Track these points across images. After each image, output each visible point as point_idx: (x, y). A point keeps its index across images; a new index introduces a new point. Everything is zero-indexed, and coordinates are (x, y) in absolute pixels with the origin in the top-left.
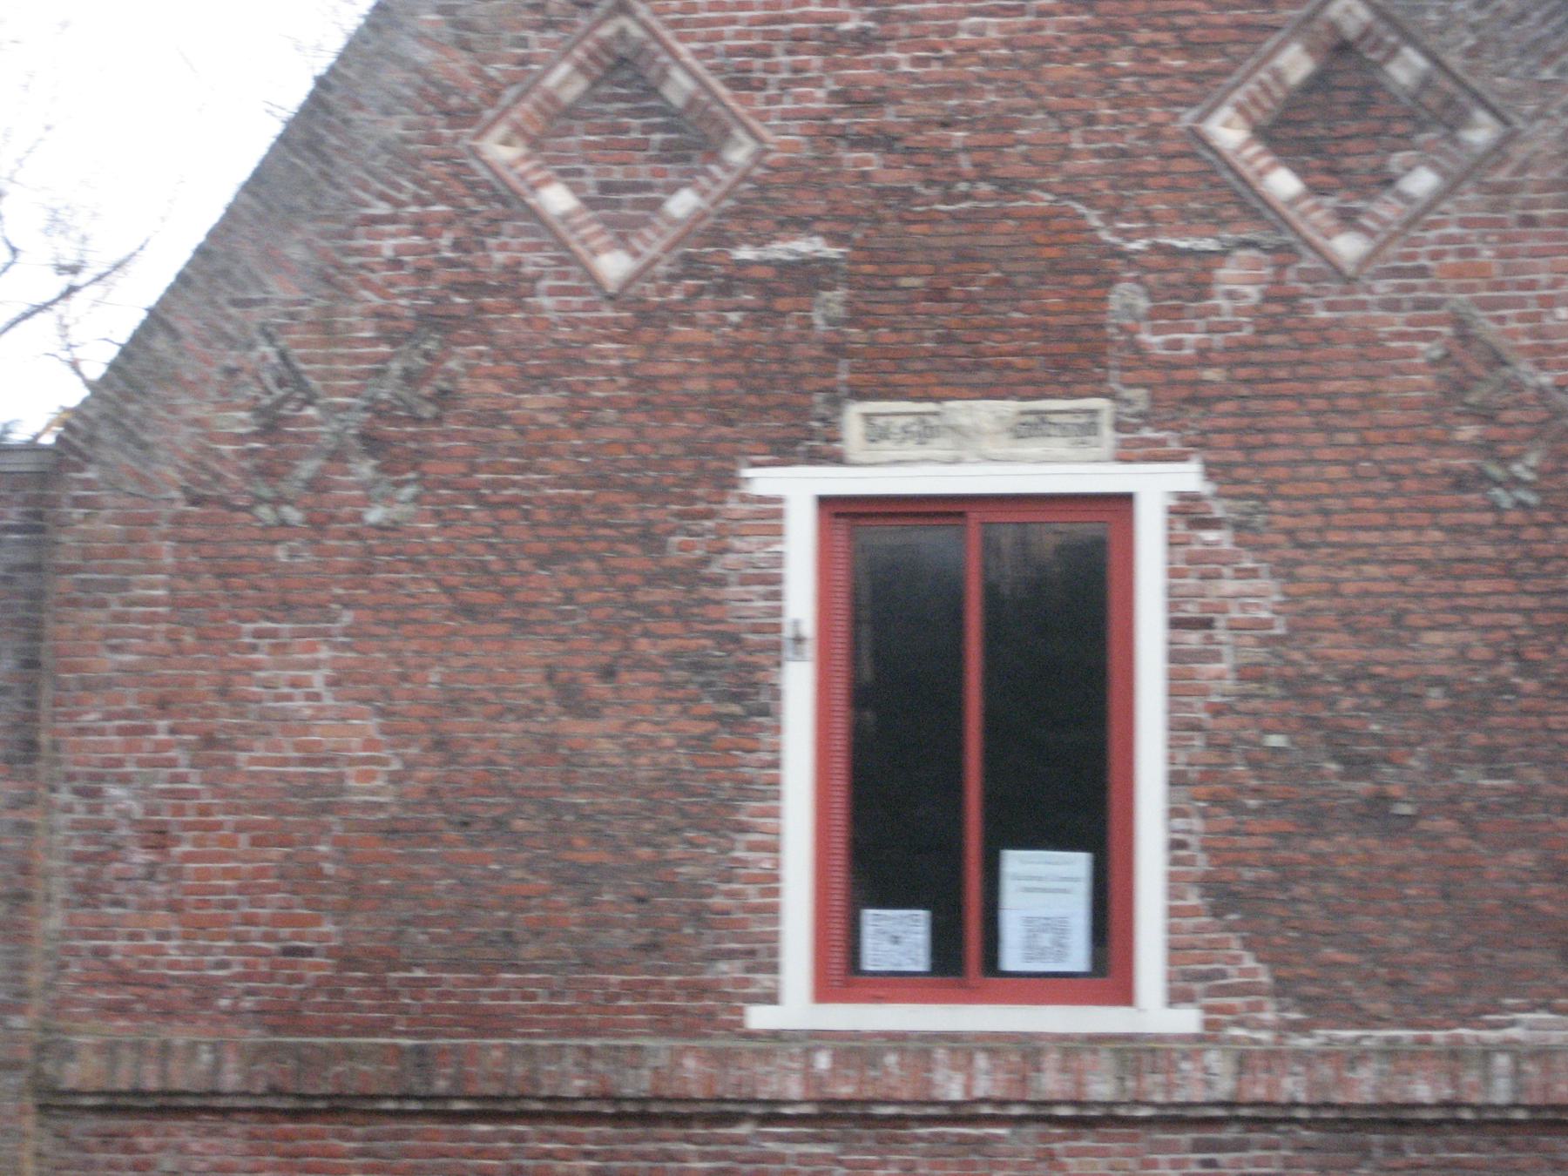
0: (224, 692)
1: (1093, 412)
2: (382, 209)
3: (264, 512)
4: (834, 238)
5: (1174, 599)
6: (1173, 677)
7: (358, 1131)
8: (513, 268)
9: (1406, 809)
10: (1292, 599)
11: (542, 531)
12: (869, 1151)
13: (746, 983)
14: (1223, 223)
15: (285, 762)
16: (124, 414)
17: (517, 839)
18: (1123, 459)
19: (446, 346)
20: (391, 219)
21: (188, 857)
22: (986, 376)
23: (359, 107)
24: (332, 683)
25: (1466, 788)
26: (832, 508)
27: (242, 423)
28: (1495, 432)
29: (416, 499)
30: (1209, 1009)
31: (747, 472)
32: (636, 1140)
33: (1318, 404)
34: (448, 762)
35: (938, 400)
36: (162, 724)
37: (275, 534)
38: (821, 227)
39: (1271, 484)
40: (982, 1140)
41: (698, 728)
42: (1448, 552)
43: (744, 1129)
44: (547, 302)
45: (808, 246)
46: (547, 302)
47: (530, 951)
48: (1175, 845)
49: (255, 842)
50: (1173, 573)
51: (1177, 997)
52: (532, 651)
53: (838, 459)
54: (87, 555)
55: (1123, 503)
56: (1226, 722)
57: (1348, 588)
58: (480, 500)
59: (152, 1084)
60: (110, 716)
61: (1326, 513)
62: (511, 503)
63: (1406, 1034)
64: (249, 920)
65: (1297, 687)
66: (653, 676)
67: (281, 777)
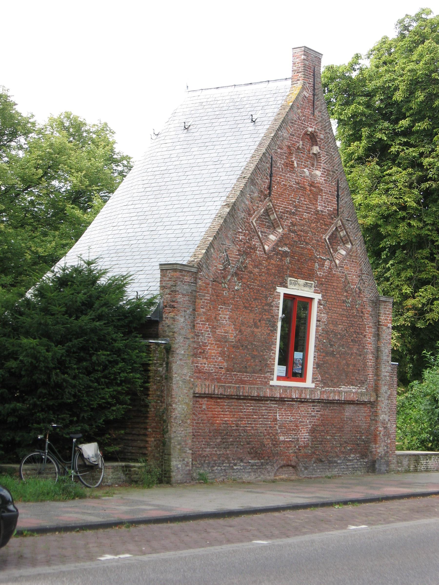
0: (215, 318)
1: (312, 284)
2: (240, 230)
3: (223, 285)
4: (289, 248)
5: (318, 316)
6: (316, 329)
7: (226, 401)
8: (255, 245)
9: (335, 353)
10: (328, 318)
11: (255, 294)
12: (281, 406)
13: (270, 377)
14: (326, 255)
15: (222, 332)
16: (207, 262)
17: (248, 349)
18: (315, 293)
19: (247, 258)
20: (241, 233)
21: (209, 349)
22: (302, 276)
23: (239, 210)
24: (229, 318)
25: (341, 350)
26: (285, 295)
27: (221, 267)
28: (348, 294)
29: (241, 286)
30: (316, 384)
31: (277, 288)
32: (231, 402)
33: (332, 287)
34: (242, 335)
35: (298, 279)
36: (207, 323)
37: (224, 289)
38: (288, 246)
39: (328, 299)
40: (293, 404)
41: (269, 332)
42: (342, 313)
43: (268, 402)
44: (258, 252)
45: (286, 249)
46: (258, 252)
47: (248, 370)
48: (315, 357)
49: (217, 347)
50: (318, 312)
51: (313, 382)
52: (252, 315)
53: (287, 287)
54: (200, 289)
55: (312, 299)
56: (320, 337)
57: (333, 317)
58: (248, 287)
59: (207, 392)
60: (201, 321)
61: (332, 305)
62: (252, 288)
63: (332, 389)
64: (216, 362)
65: (327, 332)
66: (265, 322)
67: (221, 335)
